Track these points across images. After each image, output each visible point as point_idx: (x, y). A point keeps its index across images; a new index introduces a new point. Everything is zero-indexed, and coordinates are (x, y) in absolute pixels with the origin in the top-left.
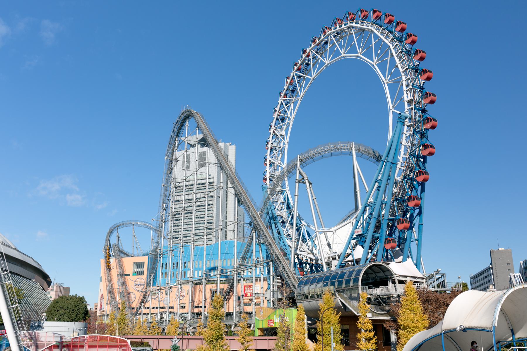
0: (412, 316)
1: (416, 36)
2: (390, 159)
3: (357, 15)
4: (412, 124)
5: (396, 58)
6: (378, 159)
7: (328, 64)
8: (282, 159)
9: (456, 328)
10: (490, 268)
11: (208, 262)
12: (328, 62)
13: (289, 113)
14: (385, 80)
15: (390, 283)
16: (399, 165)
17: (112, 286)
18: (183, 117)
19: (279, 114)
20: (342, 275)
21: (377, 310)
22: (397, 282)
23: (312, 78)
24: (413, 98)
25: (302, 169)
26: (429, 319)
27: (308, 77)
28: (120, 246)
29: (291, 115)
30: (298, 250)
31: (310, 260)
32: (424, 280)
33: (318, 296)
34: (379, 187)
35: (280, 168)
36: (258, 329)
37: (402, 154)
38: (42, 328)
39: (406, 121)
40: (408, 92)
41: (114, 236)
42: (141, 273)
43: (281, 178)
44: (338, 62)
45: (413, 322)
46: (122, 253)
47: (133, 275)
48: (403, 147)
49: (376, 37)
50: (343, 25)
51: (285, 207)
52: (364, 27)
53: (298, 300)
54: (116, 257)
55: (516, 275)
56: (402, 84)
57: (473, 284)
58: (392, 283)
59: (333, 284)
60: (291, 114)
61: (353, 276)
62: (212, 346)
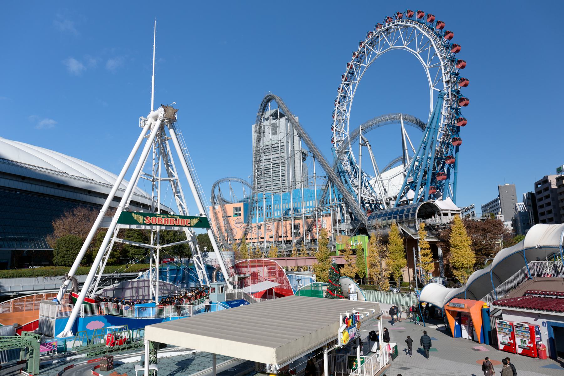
0: (460, 238)
1: (423, 12)
2: (433, 126)
3: (404, 15)
4: (450, 98)
5: (435, 48)
6: (422, 126)
7: (379, 55)
8: (345, 128)
9: (536, 247)
10: (498, 199)
11: (284, 205)
12: (379, 53)
13: (349, 93)
14: (426, 66)
15: (437, 215)
16: (440, 130)
17: (219, 225)
18: (266, 100)
19: (341, 94)
20: (402, 211)
21: (429, 235)
22: (442, 214)
23: (367, 66)
24: (450, 79)
25: (363, 135)
26: (472, 239)
27: (363, 65)
28: (221, 196)
29: (351, 95)
30: (362, 194)
31: (372, 201)
32: (460, 212)
33: (384, 226)
34: (425, 147)
35: (343, 135)
36: (339, 250)
37: (442, 122)
38: (207, 256)
39: (445, 96)
40: (446, 74)
41: (217, 189)
42: (239, 215)
43: (346, 142)
44: (387, 53)
45: (460, 242)
46: (224, 202)
47: (234, 216)
48: (443, 117)
49: (418, 32)
50: (391, 23)
51: (349, 163)
52: (409, 24)
53: (369, 229)
54: (220, 204)
55: (520, 203)
56: (441, 69)
57: (484, 211)
58: (438, 215)
59: (395, 218)
60: (350, 94)
61: (411, 212)
62: (322, 263)
